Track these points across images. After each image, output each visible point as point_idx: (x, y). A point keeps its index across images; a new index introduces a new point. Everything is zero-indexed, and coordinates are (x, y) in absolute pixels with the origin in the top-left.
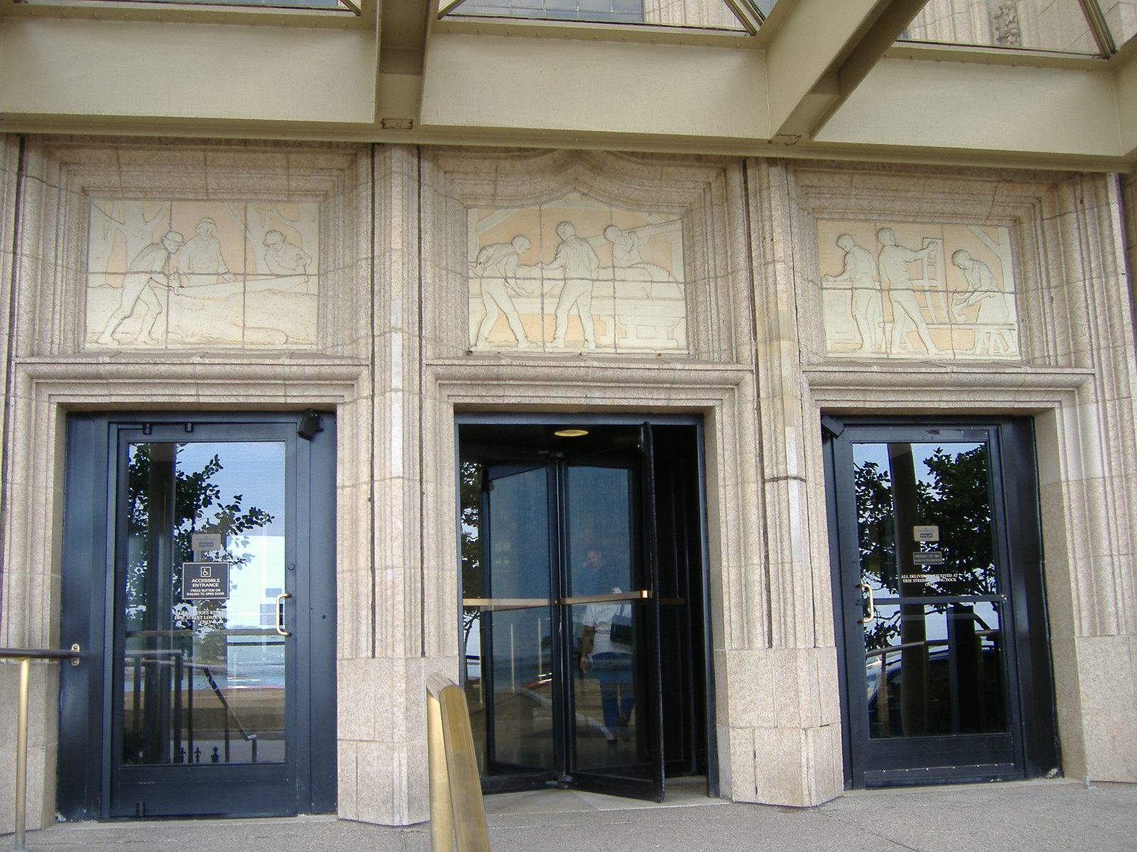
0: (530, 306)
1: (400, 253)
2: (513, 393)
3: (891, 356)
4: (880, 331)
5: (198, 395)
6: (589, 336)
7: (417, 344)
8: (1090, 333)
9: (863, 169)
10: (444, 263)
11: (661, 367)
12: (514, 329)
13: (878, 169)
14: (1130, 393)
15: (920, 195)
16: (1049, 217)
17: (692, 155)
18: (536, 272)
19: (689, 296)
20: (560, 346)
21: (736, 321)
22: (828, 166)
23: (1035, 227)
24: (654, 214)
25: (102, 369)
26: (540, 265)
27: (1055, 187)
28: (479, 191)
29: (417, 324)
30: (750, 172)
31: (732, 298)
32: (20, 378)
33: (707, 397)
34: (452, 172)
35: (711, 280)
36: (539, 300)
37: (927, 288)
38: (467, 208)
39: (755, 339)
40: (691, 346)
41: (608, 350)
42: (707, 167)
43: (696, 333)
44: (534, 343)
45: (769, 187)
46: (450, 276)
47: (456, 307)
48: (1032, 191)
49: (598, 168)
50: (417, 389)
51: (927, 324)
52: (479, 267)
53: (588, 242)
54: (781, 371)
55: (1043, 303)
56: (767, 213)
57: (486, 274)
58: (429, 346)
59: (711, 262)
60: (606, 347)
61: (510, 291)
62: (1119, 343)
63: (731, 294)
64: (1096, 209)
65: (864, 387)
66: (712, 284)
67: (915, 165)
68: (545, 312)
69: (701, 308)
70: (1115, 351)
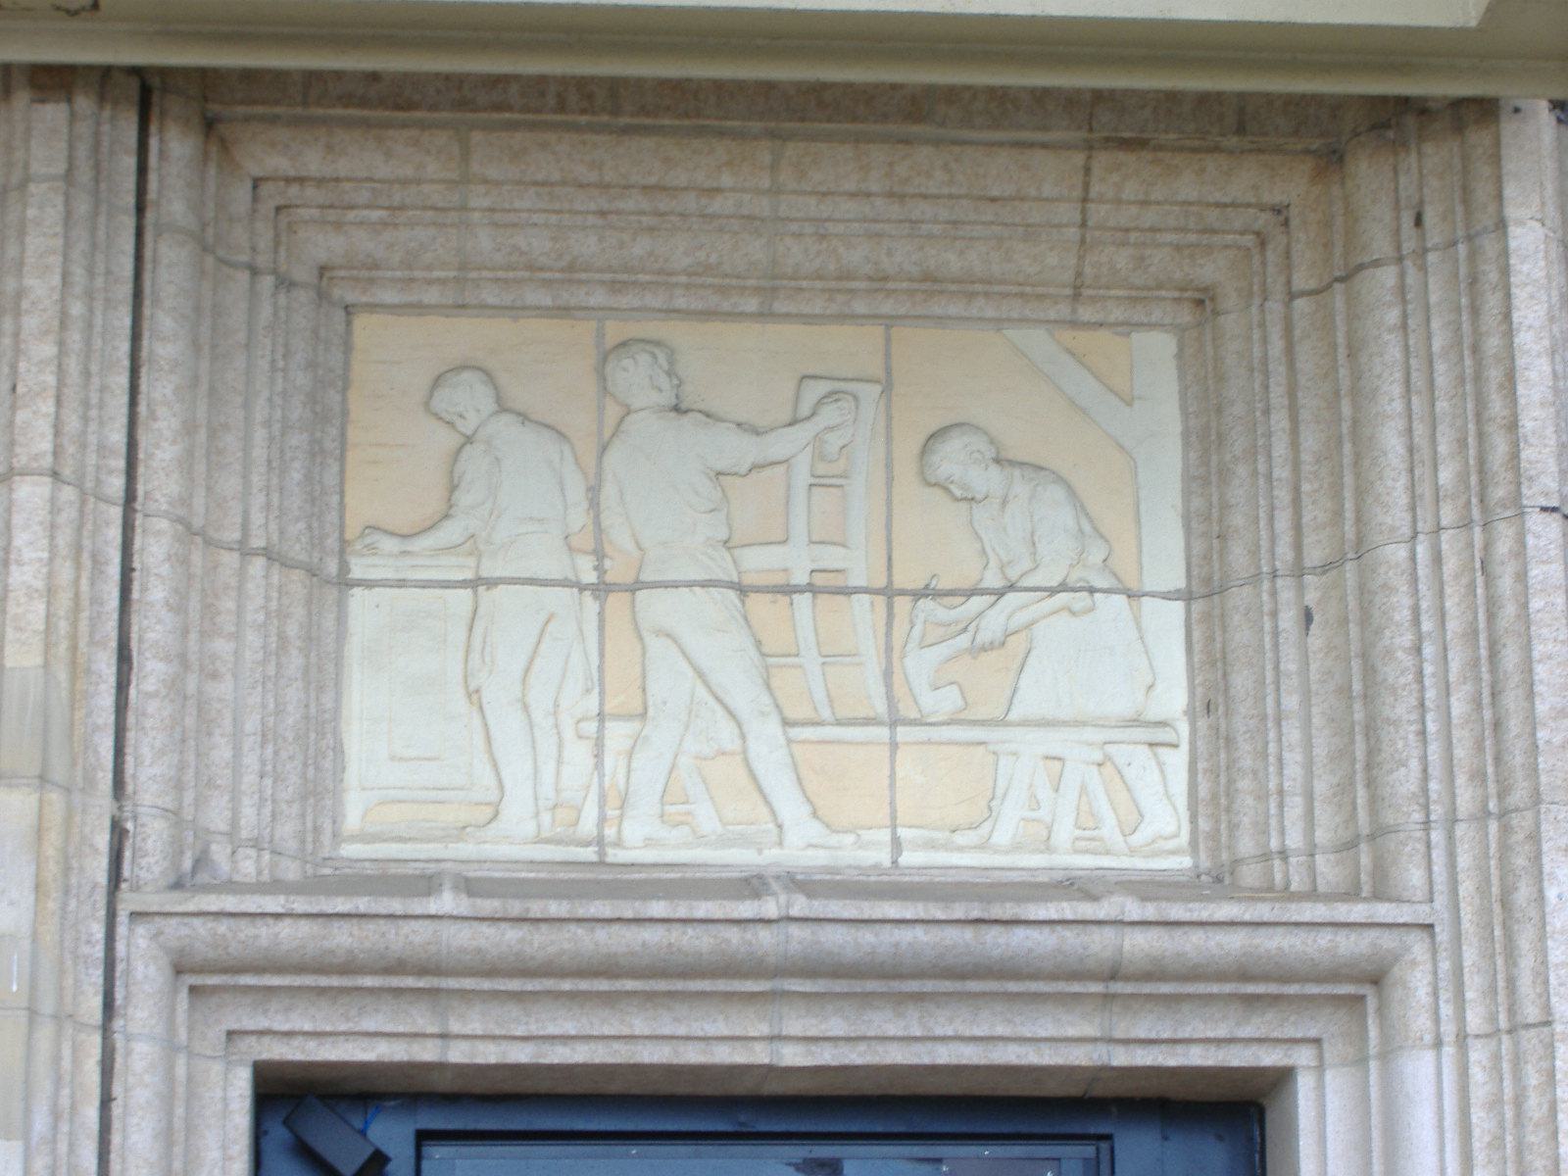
3: (615, 855)
4: (579, 754)
8: (1424, 759)
9: (498, 107)
13: (562, 107)
14: (1547, 1008)
15: (763, 206)
16: (1313, 284)
22: (347, 100)
23: (1262, 325)
27: (1332, 160)
32: (144, 959)
37: (800, 578)
48: (1247, 182)
51: (787, 723)
55: (1276, 634)
62: (1519, 795)
64: (1462, 249)
65: (421, 977)
67: (718, 85)
70: (1506, 830)
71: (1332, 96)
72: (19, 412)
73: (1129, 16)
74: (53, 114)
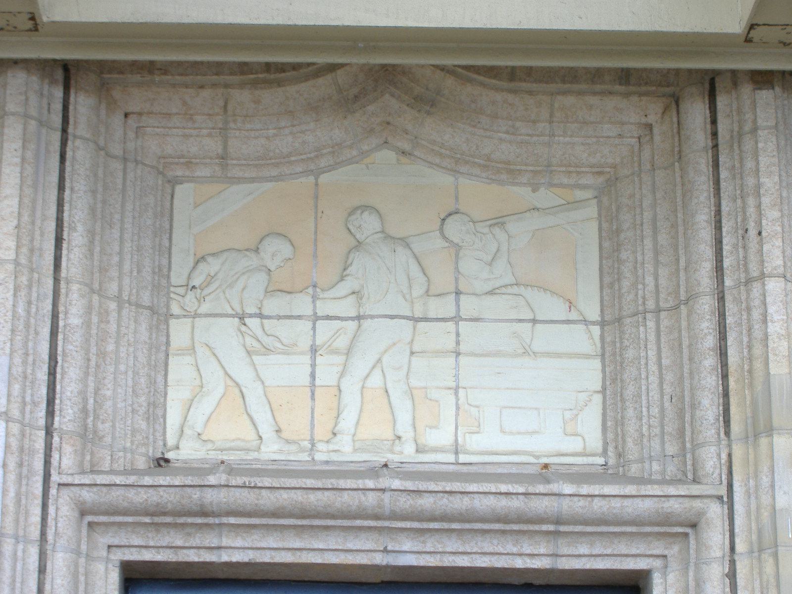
0: (287, 371)
1: (10, 267)
2: (239, 542)
5: (385, 551)
6: (404, 428)
7: (40, 445)
10: (113, 288)
11: (531, 489)
12: (255, 417)
17: (609, 70)
18: (302, 304)
19: (608, 349)
20: (345, 450)
21: (693, 396)
24: (542, 190)
25: (211, 497)
26: (310, 290)
28: (194, 150)
29: (44, 405)
30: (722, 101)
31: (685, 351)
32: (63, 509)
33: (634, 551)
34: (140, 114)
35: (649, 316)
36: (307, 359)
38: (174, 182)
39: (727, 433)
40: (611, 449)
41: (440, 457)
42: (641, 95)
43: (620, 423)
44: (294, 442)
45: (755, 130)
46: (125, 312)
47: (136, 373)
49: (426, 102)
50: (35, 533)
52: (191, 295)
53: (408, 246)
54: (774, 499)
56: (751, 181)
57: (204, 308)
58: (68, 449)
59: (650, 280)
60: (435, 450)
61: (249, 341)
63: (686, 343)
66: (651, 324)
68: (318, 382)
69: (630, 373)
71: (162, 61)
72: (764, 245)
73: (451, 26)
74: (765, 96)
